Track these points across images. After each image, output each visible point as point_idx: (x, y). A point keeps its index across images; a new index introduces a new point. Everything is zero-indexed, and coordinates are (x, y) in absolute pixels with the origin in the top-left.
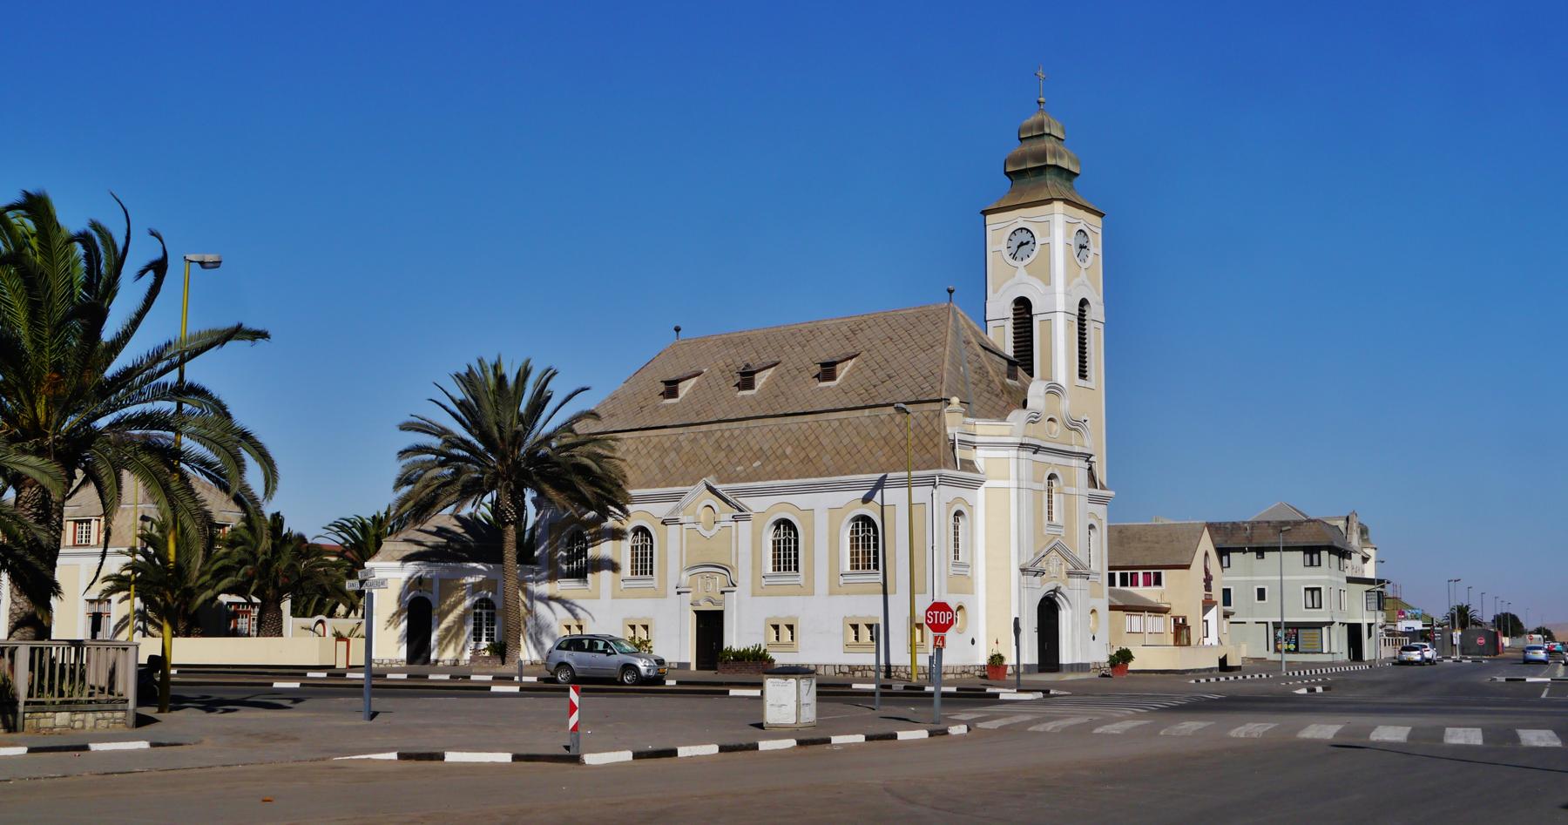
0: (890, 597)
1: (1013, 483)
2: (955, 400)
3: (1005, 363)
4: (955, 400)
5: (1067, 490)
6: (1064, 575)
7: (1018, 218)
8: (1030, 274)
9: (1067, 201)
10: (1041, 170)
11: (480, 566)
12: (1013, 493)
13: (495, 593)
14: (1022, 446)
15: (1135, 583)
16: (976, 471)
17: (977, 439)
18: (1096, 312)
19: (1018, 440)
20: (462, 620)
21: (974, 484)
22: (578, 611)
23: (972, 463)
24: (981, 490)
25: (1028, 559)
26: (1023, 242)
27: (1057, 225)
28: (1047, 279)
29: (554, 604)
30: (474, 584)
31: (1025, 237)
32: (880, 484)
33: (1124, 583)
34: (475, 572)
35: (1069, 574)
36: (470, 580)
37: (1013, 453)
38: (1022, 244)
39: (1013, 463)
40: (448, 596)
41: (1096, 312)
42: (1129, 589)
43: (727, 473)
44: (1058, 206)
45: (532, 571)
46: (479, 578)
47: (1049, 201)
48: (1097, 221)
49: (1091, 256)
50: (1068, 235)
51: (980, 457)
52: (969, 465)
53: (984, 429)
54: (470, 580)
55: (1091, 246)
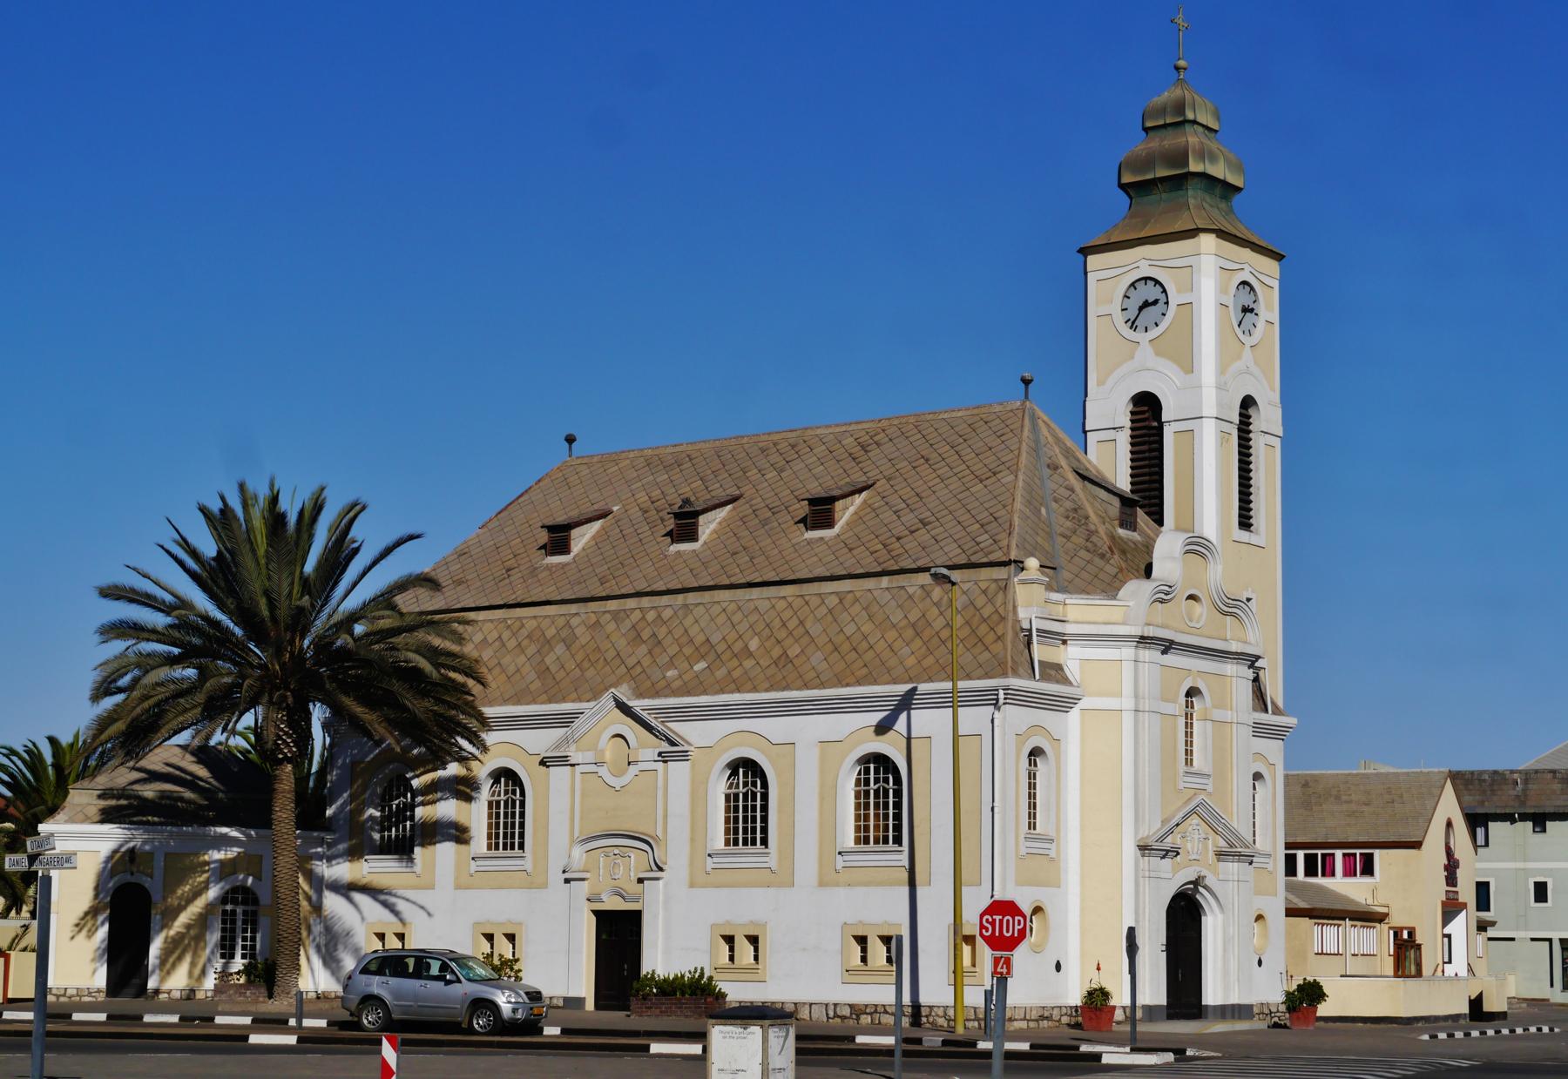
0: (920, 891)
1: (1128, 703)
2: (1032, 563)
3: (1116, 502)
4: (1032, 563)
5: (1218, 714)
6: (1211, 856)
7: (1142, 261)
8: (1158, 354)
9: (1222, 234)
10: (1180, 181)
11: (234, 833)
12: (1128, 719)
13: (258, 878)
14: (1144, 640)
15: (1329, 871)
16: (1070, 684)
17: (1069, 629)
18: (1268, 418)
19: (1137, 631)
20: (203, 921)
21: (1063, 704)
22: (401, 905)
23: (1058, 668)
24: (1075, 713)
25: (1151, 829)
26: (1148, 302)
27: (1205, 272)
28: (1188, 364)
29: (358, 897)
30: (220, 861)
31: (1152, 292)
32: (906, 703)
33: (1311, 871)
34: (226, 841)
35: (1220, 855)
36: (217, 855)
37: (1128, 652)
38: (1146, 304)
39: (1128, 668)
40: (181, 881)
41: (1268, 418)
42: (1319, 880)
43: (655, 680)
44: (1208, 241)
45: (321, 842)
46: (232, 852)
47: (1192, 233)
48: (1271, 267)
49: (1261, 324)
50: (1222, 290)
51: (1072, 657)
52: (1054, 671)
53: (1081, 612)
54: (217, 855)
55: (1261, 308)
